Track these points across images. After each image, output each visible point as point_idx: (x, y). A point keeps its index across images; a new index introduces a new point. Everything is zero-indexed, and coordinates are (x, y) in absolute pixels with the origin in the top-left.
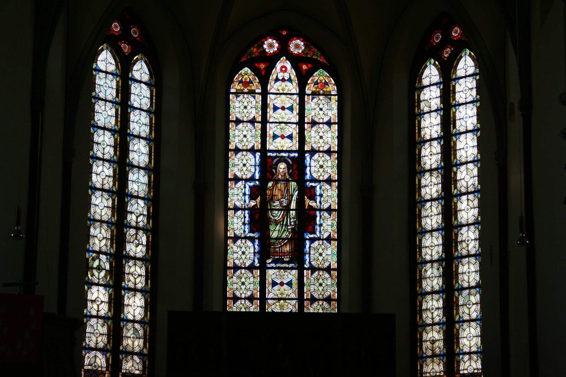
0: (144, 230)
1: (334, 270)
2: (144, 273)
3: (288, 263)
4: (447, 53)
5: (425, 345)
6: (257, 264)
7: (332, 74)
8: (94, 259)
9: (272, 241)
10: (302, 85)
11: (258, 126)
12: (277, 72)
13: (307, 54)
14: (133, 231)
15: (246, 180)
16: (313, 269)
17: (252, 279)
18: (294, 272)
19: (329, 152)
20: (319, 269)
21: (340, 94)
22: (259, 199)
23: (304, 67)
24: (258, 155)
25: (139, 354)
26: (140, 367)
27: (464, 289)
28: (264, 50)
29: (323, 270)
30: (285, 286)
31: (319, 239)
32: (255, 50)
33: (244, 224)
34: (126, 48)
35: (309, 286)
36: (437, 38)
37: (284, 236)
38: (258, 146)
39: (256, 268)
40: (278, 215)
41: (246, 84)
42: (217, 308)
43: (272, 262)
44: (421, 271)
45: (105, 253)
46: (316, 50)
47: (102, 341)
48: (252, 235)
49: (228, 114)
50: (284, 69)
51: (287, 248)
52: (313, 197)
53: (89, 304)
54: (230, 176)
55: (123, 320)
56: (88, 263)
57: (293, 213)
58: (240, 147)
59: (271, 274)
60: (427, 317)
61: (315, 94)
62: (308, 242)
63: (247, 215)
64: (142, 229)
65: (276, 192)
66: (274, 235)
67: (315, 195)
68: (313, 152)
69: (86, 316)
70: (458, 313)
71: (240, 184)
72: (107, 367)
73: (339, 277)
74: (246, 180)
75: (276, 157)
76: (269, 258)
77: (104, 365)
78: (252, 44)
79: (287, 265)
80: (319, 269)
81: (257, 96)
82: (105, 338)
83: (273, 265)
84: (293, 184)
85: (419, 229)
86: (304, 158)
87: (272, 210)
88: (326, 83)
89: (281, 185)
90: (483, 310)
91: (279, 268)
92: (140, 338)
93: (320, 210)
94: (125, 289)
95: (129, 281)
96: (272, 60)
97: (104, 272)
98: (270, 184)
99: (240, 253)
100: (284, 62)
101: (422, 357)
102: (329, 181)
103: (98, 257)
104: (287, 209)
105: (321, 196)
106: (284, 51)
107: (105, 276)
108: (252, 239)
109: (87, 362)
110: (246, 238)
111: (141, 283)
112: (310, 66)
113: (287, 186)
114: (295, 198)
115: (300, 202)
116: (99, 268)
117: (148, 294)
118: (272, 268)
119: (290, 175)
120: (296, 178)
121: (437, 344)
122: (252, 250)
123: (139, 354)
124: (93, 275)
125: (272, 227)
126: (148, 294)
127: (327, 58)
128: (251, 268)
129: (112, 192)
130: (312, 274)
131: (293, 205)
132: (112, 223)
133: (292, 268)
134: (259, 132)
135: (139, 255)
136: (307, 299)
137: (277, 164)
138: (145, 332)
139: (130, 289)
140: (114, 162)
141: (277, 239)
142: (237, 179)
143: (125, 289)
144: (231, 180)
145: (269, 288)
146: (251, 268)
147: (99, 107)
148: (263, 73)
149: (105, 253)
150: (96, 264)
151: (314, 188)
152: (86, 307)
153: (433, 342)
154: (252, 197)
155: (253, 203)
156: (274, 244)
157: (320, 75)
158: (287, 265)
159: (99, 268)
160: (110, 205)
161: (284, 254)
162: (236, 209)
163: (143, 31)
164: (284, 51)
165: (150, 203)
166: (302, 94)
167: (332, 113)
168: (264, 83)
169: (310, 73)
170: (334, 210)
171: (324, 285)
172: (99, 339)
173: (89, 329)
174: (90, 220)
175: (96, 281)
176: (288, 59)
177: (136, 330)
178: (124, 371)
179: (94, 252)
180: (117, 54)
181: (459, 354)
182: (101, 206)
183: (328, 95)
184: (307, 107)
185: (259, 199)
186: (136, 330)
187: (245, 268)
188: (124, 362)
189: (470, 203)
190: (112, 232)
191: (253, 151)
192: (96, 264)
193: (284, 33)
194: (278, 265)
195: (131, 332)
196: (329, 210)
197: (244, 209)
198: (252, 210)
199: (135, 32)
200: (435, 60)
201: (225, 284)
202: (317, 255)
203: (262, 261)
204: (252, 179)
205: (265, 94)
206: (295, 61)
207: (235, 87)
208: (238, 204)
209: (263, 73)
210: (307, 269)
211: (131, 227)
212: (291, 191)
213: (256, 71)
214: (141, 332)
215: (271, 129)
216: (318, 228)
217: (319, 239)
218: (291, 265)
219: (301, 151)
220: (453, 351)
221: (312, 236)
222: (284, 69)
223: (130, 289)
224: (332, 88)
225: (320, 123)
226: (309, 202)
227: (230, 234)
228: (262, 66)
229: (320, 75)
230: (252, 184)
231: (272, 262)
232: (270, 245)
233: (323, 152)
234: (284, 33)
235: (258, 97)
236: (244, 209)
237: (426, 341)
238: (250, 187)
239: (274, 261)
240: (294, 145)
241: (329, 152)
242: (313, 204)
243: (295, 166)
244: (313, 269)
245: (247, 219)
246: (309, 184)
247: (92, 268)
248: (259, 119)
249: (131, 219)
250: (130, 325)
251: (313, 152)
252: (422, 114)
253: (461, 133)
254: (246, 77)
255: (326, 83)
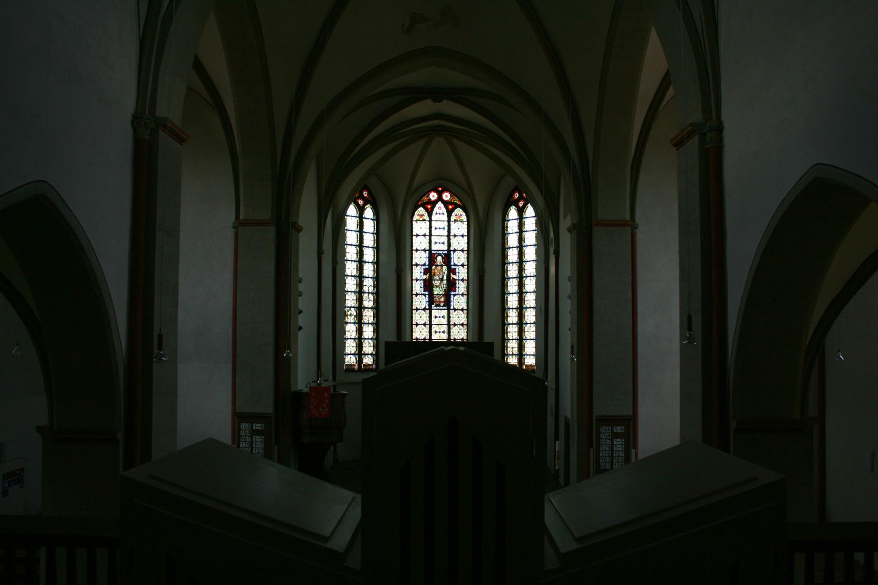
0: (372, 293)
1: (465, 310)
2: (372, 315)
3: (443, 306)
4: (521, 204)
5: (509, 349)
6: (427, 307)
7: (465, 210)
8: (348, 311)
9: (435, 296)
10: (449, 216)
11: (428, 238)
12: (436, 210)
13: (451, 200)
14: (366, 295)
15: (422, 265)
16: (455, 310)
17: (425, 315)
18: (446, 311)
19: (462, 251)
20: (458, 310)
21: (468, 221)
22: (428, 274)
23: (450, 207)
24: (427, 252)
25: (371, 354)
26: (372, 361)
27: (527, 324)
28: (430, 199)
29: (460, 310)
30: (441, 333)
31: (458, 294)
32: (426, 198)
33: (421, 287)
34: (361, 202)
35: (453, 318)
36: (517, 196)
37: (440, 293)
38: (427, 248)
39: (427, 309)
40: (437, 283)
41: (421, 216)
42: (408, 339)
43: (435, 306)
44: (507, 313)
45: (354, 307)
46: (456, 198)
47: (353, 350)
48: (424, 293)
49: (412, 231)
50: (440, 208)
51: (442, 299)
52: (455, 274)
53: (347, 332)
54: (414, 263)
55: (363, 339)
56: (345, 313)
57: (445, 282)
58: (418, 307)
59: (434, 312)
60: (510, 336)
61: (455, 221)
62: (452, 296)
63: (422, 283)
64: (371, 293)
65: (436, 271)
66: (435, 293)
67: (456, 272)
68: (455, 251)
69: (346, 339)
70: (524, 335)
71: (419, 267)
72: (356, 362)
73: (467, 314)
74: (422, 265)
75: (437, 253)
76: (433, 304)
77: (355, 361)
78: (424, 196)
79: (442, 308)
80: (458, 310)
81: (426, 222)
82: (355, 349)
83: (435, 308)
84: (445, 267)
85: (506, 292)
86: (450, 254)
87: (434, 280)
88: (461, 215)
89: (439, 268)
90: (536, 335)
91: (438, 309)
92: (371, 347)
93: (458, 280)
94: (363, 323)
95: (365, 319)
96: (434, 203)
97: (353, 316)
98: (434, 267)
99: (419, 302)
100: (440, 204)
101: (507, 355)
102: (463, 265)
103: (350, 310)
104: (442, 280)
105: (459, 273)
106: (440, 199)
107: (354, 319)
108: (425, 295)
109: (346, 361)
110: (422, 294)
111: (371, 320)
112: (453, 206)
113: (442, 268)
114: (446, 274)
115: (449, 276)
116: (351, 315)
117: (375, 325)
118: (435, 309)
119: (443, 262)
120: (446, 264)
121: (514, 349)
122: (425, 301)
123: (371, 354)
124: (348, 319)
125: (434, 289)
126: (375, 325)
127: (461, 202)
128: (424, 309)
129: (356, 276)
130: (454, 312)
131: (445, 278)
132: (356, 292)
133: (445, 309)
134: (428, 315)
135: (370, 306)
136: (452, 325)
137: (437, 256)
138: (374, 343)
139: (366, 323)
140: (357, 261)
141: (437, 295)
142: (417, 265)
143: (363, 323)
144: (414, 265)
145: (433, 319)
146: (424, 309)
147: (348, 234)
148: (430, 210)
149: (354, 307)
150: (349, 313)
151: (455, 269)
152: (345, 335)
153: (513, 348)
154: (425, 274)
155: (425, 277)
156: (435, 297)
157: (458, 211)
158: (442, 308)
159: (351, 315)
160: (355, 283)
161: (441, 302)
162: (417, 280)
163: (370, 193)
164: (440, 199)
165: (375, 280)
166: (449, 221)
167: (464, 231)
168: (430, 215)
169: (453, 210)
170: (465, 280)
171: (460, 317)
172: (352, 349)
173: (347, 345)
174: (346, 292)
175: (350, 321)
176: (442, 203)
177: (369, 343)
178: (364, 363)
179: (348, 307)
180: (357, 204)
181: (525, 355)
182: (351, 284)
183: (462, 221)
184: (451, 227)
185: (428, 274)
186: (369, 343)
187: (422, 309)
188: (364, 359)
189: (531, 281)
190: (357, 296)
191: (425, 250)
192: (349, 313)
193: (440, 189)
194: (438, 308)
195: (367, 344)
196: (463, 280)
197: (421, 280)
198: (425, 280)
199: (365, 194)
200: (515, 206)
201: (412, 317)
202: (457, 302)
203: (430, 306)
204: (425, 265)
205: (430, 221)
206: (446, 204)
207: (416, 217)
208: (418, 292)
209: (430, 210)
210: (452, 310)
211: (365, 293)
212: (444, 271)
213: (426, 210)
214: (372, 344)
215: (434, 239)
216: (457, 289)
217: (458, 294)
218: (444, 308)
219: (449, 250)
220: (522, 353)
221: (455, 293)
222: (440, 208)
223: (366, 323)
224: (464, 218)
225: (460, 325)
226: (453, 276)
227: (414, 292)
228: (429, 207)
229: (458, 211)
230: (424, 267)
231: (435, 306)
232: (434, 298)
233: (460, 250)
234: (440, 189)
235: (428, 223)
236: (421, 280)
237: (509, 347)
238: (424, 269)
239: (436, 306)
240: (445, 247)
241: (462, 251)
242: (454, 277)
243: (446, 258)
244: (455, 310)
245: (422, 285)
246: (453, 267)
247: (348, 315)
248: (428, 234)
249: (365, 289)
250: (366, 341)
251: (455, 251)
252: (508, 234)
253: (527, 308)
254: (421, 212)
255: (461, 215)
